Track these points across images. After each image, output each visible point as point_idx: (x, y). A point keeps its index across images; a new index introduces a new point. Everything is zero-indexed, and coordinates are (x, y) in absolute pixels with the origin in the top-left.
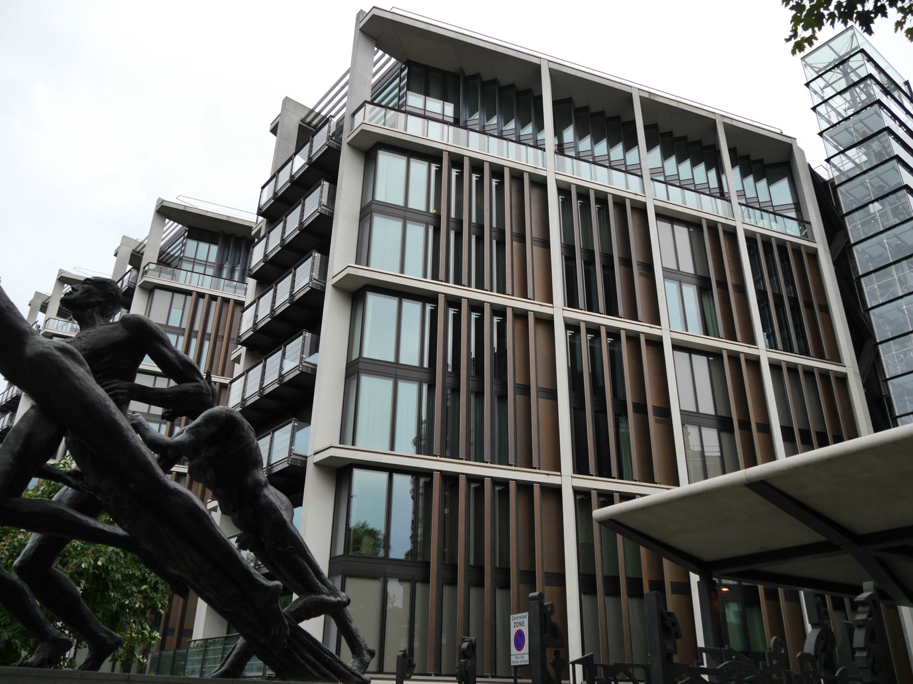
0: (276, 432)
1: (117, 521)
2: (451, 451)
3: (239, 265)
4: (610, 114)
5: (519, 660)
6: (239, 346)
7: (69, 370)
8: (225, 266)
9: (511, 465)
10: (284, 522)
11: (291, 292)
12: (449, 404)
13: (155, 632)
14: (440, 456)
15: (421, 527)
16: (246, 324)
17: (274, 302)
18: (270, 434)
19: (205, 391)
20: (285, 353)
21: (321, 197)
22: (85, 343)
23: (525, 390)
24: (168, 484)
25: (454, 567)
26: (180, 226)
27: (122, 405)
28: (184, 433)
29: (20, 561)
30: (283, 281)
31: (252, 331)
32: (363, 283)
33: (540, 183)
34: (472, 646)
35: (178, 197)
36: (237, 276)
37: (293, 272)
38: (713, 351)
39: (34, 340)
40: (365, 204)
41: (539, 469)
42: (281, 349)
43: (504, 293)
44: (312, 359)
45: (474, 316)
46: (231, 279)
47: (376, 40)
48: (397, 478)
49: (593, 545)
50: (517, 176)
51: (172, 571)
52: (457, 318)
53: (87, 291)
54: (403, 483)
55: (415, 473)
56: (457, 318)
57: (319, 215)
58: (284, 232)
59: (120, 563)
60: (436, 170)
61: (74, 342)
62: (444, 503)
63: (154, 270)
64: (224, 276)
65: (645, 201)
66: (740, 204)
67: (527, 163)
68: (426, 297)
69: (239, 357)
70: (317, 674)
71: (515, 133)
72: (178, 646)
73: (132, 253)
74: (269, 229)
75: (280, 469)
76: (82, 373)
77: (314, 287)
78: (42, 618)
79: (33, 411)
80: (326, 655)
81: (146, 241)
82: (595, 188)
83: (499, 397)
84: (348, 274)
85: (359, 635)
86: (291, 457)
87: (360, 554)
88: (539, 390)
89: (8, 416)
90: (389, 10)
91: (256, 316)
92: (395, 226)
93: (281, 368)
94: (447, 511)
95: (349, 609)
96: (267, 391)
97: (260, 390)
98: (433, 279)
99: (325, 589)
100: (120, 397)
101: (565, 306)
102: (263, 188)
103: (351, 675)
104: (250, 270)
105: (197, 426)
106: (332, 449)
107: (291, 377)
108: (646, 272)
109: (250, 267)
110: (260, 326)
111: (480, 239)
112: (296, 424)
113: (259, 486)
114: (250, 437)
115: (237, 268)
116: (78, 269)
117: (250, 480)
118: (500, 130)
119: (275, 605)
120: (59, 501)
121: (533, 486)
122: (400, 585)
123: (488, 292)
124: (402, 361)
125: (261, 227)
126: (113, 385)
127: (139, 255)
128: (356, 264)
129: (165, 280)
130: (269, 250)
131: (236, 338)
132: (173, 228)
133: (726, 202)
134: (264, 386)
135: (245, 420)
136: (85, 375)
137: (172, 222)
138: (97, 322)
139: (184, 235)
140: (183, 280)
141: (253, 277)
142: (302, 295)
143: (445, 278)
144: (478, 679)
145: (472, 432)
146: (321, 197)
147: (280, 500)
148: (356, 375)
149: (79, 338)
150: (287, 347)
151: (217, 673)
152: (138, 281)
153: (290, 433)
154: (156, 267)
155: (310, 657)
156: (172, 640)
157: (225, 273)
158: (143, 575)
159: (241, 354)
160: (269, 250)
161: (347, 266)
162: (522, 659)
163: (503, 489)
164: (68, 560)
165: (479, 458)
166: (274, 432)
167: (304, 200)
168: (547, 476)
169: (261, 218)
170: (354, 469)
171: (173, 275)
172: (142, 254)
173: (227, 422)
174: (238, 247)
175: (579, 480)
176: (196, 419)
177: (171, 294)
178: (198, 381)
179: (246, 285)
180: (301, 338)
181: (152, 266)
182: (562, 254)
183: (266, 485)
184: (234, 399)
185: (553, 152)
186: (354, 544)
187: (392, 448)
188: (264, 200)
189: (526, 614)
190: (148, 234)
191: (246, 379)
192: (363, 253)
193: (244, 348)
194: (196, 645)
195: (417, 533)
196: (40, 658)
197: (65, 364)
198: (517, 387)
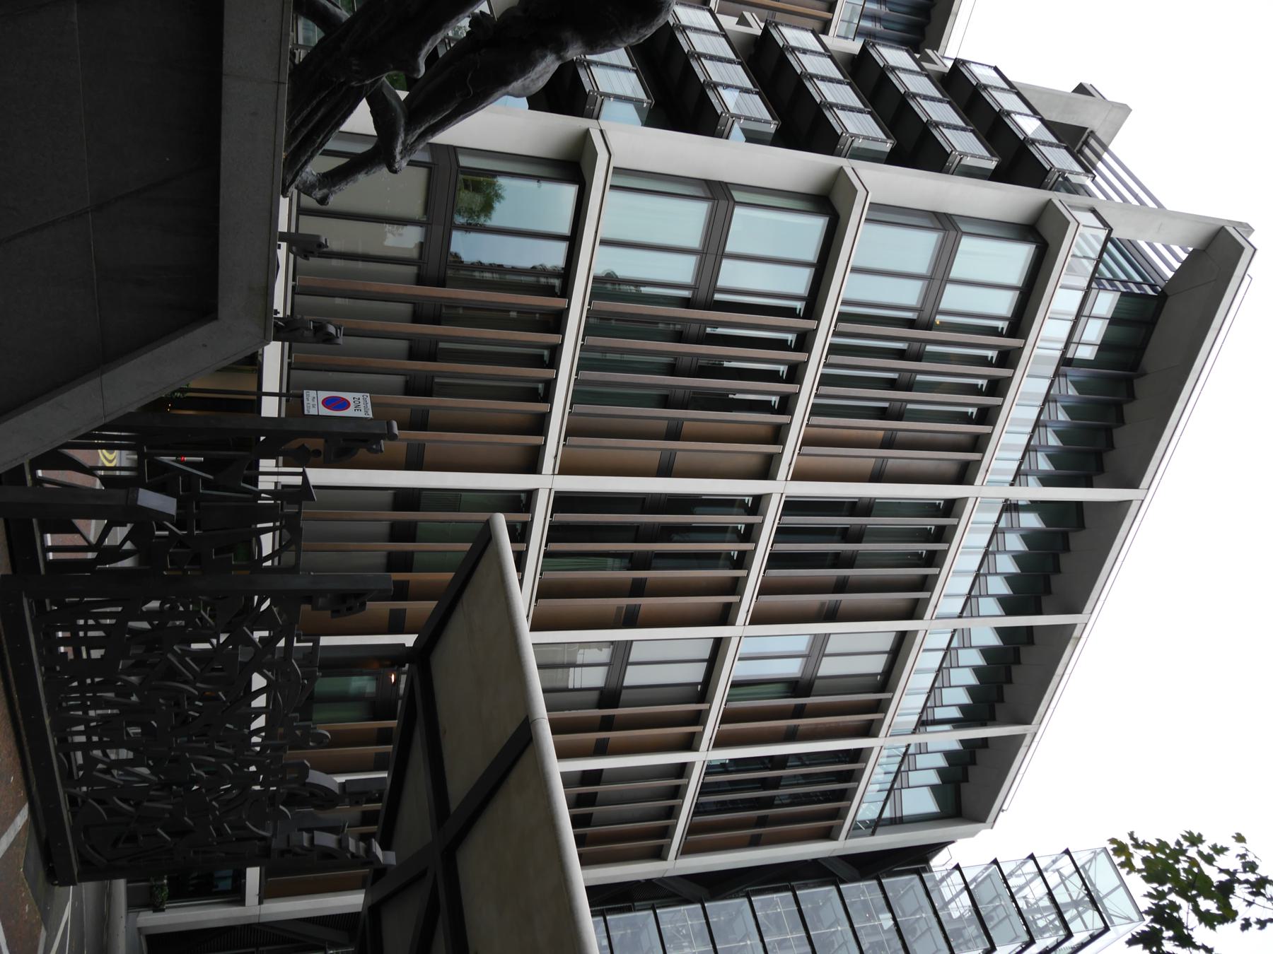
2: (595, 325)
4: (1056, 581)
5: (310, 401)
9: (571, 408)
10: (506, 83)
12: (661, 326)
14: (588, 310)
15: (493, 277)
17: (824, 79)
18: (633, 66)
21: (973, 156)
23: (674, 433)
25: (436, 321)
34: (329, 339)
38: (891, 682)
41: (564, 445)
43: (812, 414)
44: (737, 132)
45: (782, 369)
46: (863, 16)
47: (1204, 251)
48: (562, 247)
50: (978, 444)
54: (554, 256)
62: (523, 310)
66: (909, 745)
68: (814, 302)
75: (583, 79)
83: (666, 397)
84: (856, 191)
85: (349, 185)
86: (599, 96)
87: (460, 190)
88: (673, 453)
91: (805, 51)
94: (513, 314)
96: (694, 64)
97: (698, 54)
98: (840, 313)
99: (411, 139)
101: (786, 497)
102: (996, 69)
104: (874, 45)
106: (607, 156)
108: (825, 611)
109: (879, 44)
111: (891, 384)
112: (645, 105)
113: (559, 48)
114: (628, 37)
117: (567, 35)
124: (726, 264)
125: (936, 64)
128: (870, 203)
130: (902, 75)
134: (702, 59)
135: (654, 30)
141: (864, 49)
143: (840, 332)
146: (973, 156)
147: (538, 78)
148: (710, 196)
150: (757, 96)
159: (751, 27)
163: (540, 394)
165: (584, 364)
166: (636, 72)
169: (949, 64)
179: (853, 37)
183: (559, 58)
185: (1007, 496)
187: (605, 242)
188: (977, 70)
191: (714, 33)
192: (885, 214)
193: (758, 32)
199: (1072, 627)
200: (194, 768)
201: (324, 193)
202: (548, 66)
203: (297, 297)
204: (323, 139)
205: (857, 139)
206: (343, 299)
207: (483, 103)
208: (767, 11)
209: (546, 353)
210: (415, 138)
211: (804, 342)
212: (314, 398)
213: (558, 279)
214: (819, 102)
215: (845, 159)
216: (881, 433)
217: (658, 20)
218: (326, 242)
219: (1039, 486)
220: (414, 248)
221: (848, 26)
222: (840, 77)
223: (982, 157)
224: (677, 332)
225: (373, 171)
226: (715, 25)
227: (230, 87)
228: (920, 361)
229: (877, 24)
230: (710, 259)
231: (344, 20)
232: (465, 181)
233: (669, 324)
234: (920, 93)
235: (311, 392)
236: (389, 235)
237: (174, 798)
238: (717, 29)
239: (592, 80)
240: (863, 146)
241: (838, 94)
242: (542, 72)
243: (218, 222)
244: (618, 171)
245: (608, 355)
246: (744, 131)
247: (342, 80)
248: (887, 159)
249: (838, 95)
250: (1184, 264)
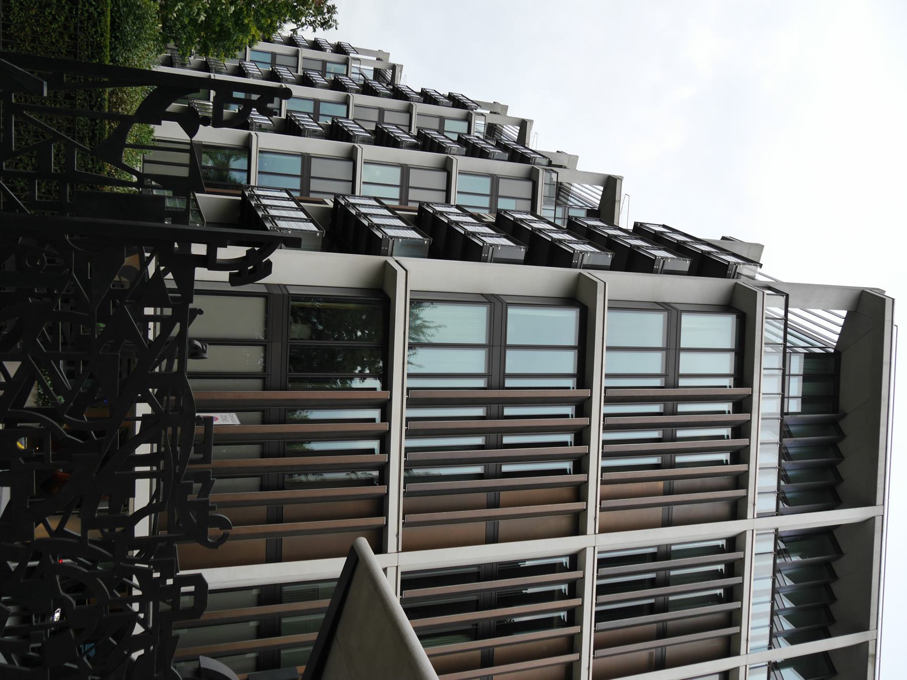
4: (835, 609)
13: (205, 15)
33: (730, 648)
45: (564, 587)
47: (856, 311)
49: (318, 599)
50: (733, 619)
60: (719, 546)
63: (551, 178)
65: (741, 654)
67: (751, 629)
68: (583, 376)
71: (780, 610)
82: (746, 558)
83: (478, 573)
84: (596, 283)
87: (291, 324)
90: (895, 323)
92: (657, 338)
106: (405, 272)
108: (654, 663)
118: (780, 591)
123: (594, 601)
124: (510, 354)
133: (768, 643)
168: (396, 533)
170: (379, 441)
175: (403, 313)
185: (769, 660)
192: (618, 306)
199: (866, 644)
200: (61, 591)
219: (788, 645)
230: (496, 351)
237: (39, 43)
250: (844, 327)
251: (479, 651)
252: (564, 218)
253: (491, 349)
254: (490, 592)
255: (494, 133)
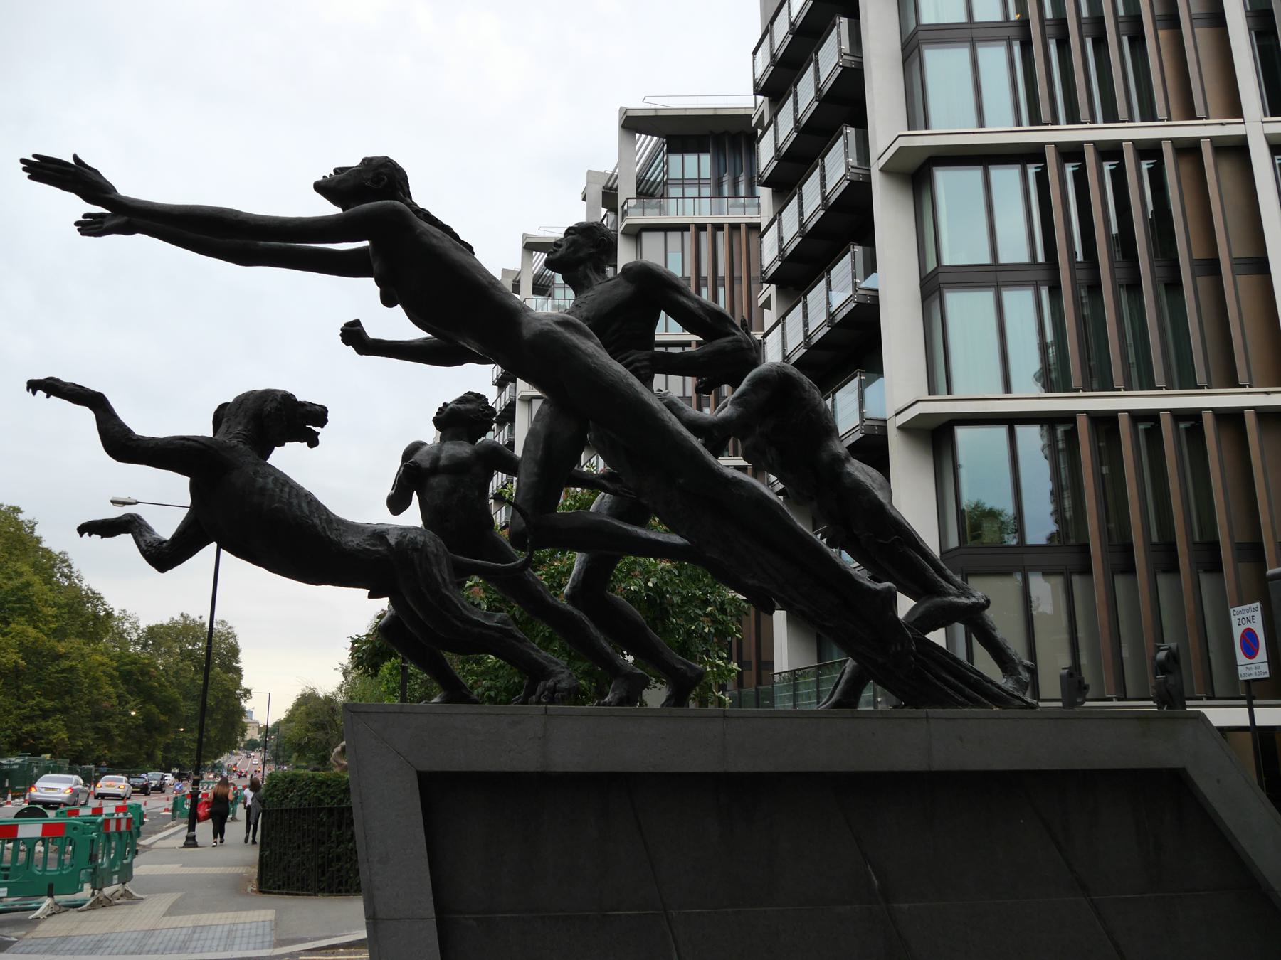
0: (837, 393)
1: (673, 529)
2: (1099, 379)
3: (743, 174)
5: (1252, 672)
6: (764, 284)
7: (576, 347)
8: (724, 179)
9: (1202, 387)
10: (881, 505)
11: (823, 193)
12: (1086, 311)
14: (1084, 391)
15: (1068, 497)
16: (769, 253)
17: (801, 214)
18: (829, 397)
19: (745, 345)
20: (830, 281)
21: (840, 43)
22: (586, 311)
23: (1210, 266)
24: (724, 473)
25: (1128, 549)
26: (655, 138)
27: (647, 381)
28: (729, 406)
29: (570, 588)
30: (806, 184)
31: (780, 261)
32: (923, 157)
34: (1173, 657)
35: (639, 103)
36: (742, 189)
37: (820, 164)
39: (529, 318)
40: (907, 36)
41: (1250, 386)
42: (824, 277)
43: (1154, 118)
44: (869, 283)
46: (736, 195)
48: (1021, 430)
51: (750, 582)
52: (1081, 178)
53: (573, 244)
54: (1030, 437)
55: (1047, 420)
56: (1081, 178)
57: (842, 71)
58: (796, 110)
59: (676, 583)
61: (573, 312)
62: (1099, 459)
63: (635, 207)
64: (726, 194)
69: (768, 301)
70: (961, 699)
72: (759, 682)
73: (603, 192)
74: (775, 111)
75: (852, 442)
76: (592, 347)
77: (855, 178)
78: (610, 652)
79: (546, 406)
80: (972, 675)
81: (617, 171)
83: (1167, 286)
84: (901, 148)
85: (1009, 646)
86: (864, 424)
87: (983, 543)
88: (1235, 262)
89: (506, 428)
91: (781, 239)
93: (829, 304)
94: (1105, 470)
95: (990, 614)
96: (815, 340)
97: (805, 339)
98: (1032, 124)
99: (953, 589)
100: (643, 372)
101: (1266, 116)
102: (755, 53)
103: (1008, 697)
104: (760, 176)
105: (742, 394)
106: (920, 404)
107: (845, 314)
109: (758, 171)
110: (789, 251)
111: (1100, 42)
112: (863, 378)
113: (838, 461)
114: (815, 398)
115: (741, 179)
116: (543, 229)
117: (824, 456)
119: (890, 614)
120: (598, 512)
121: (1243, 414)
122: (1046, 582)
124: (1004, 259)
125: (763, 111)
126: (631, 358)
127: (612, 191)
128: (909, 130)
129: (651, 217)
130: (781, 141)
131: (759, 275)
132: (647, 143)
134: (809, 333)
135: (803, 377)
136: (596, 351)
137: (643, 136)
138: (594, 282)
139: (662, 149)
140: (678, 210)
141: (765, 184)
142: (838, 194)
143: (1052, 117)
144: (1188, 703)
145: (1129, 348)
146: (840, 43)
147: (870, 477)
148: (937, 293)
149: (577, 306)
150: (831, 272)
151: (827, 704)
152: (619, 226)
153: (857, 391)
154: (637, 202)
155: (949, 677)
156: (750, 676)
157: (726, 190)
158: (705, 594)
159: (770, 295)
160: (781, 141)
161: (897, 135)
162: (1257, 671)
163: (1192, 425)
164: (614, 586)
165: (1147, 383)
166: (834, 393)
167: (816, 54)
169: (760, 98)
170: (955, 427)
171: (660, 207)
172: (616, 189)
173: (779, 383)
174: (736, 149)
176: (740, 384)
177: (662, 234)
178: (734, 334)
179: (757, 199)
180: (849, 256)
181: (632, 203)
182: (1250, 30)
183: (847, 460)
184: (773, 355)
186: (971, 532)
187: (1008, 388)
188: (760, 71)
189: (1258, 604)
190: (617, 160)
191: (783, 329)
192: (917, 112)
193: (773, 287)
194: (782, 679)
195: (1064, 506)
196: (617, 696)
197: (571, 340)
198: (1196, 265)
201: (1023, 670)
202: (857, 469)
203: (1129, 695)
204: (973, 673)
205: (850, 164)
206: (1123, 649)
207: (905, 525)
208: (752, 286)
209: (1141, 427)
210: (951, 586)
211: (1071, 152)
212: (1247, 668)
213: (1056, 429)
214: (824, 212)
215: (872, 169)
216: (1161, 33)
217: (795, 375)
218: (1065, 669)
220: (1049, 582)
221: (748, 207)
222: (796, 198)
223: (839, 34)
224: (1089, 292)
225: (990, 624)
226: (776, 329)
227: (941, 762)
228: (1066, 19)
229: (740, 180)
231: (855, 663)
232: (974, 538)
233: (1082, 303)
234: (792, 117)
235: (1240, 672)
236: (1040, 610)
238: (780, 326)
239: (851, 433)
240: (855, 156)
241: (811, 195)
242: (863, 473)
243: (1077, 771)
244: (932, 390)
245: (1131, 362)
246: (866, 276)
247: (913, 659)
248: (863, 128)
249: (810, 198)
251: (1198, 279)
252: (683, 184)
253: (1001, 284)
254: (1156, 269)
255: (543, 285)
